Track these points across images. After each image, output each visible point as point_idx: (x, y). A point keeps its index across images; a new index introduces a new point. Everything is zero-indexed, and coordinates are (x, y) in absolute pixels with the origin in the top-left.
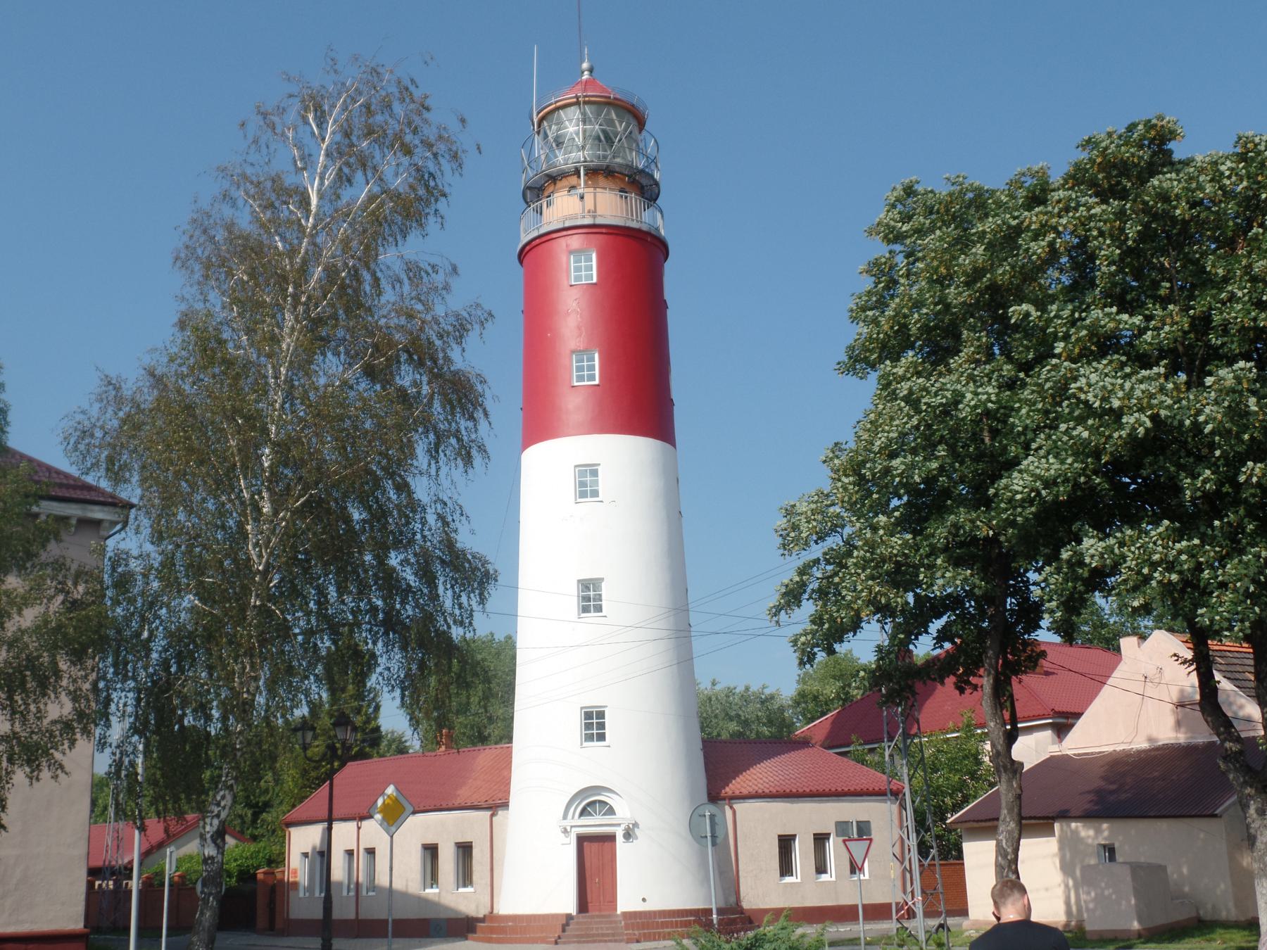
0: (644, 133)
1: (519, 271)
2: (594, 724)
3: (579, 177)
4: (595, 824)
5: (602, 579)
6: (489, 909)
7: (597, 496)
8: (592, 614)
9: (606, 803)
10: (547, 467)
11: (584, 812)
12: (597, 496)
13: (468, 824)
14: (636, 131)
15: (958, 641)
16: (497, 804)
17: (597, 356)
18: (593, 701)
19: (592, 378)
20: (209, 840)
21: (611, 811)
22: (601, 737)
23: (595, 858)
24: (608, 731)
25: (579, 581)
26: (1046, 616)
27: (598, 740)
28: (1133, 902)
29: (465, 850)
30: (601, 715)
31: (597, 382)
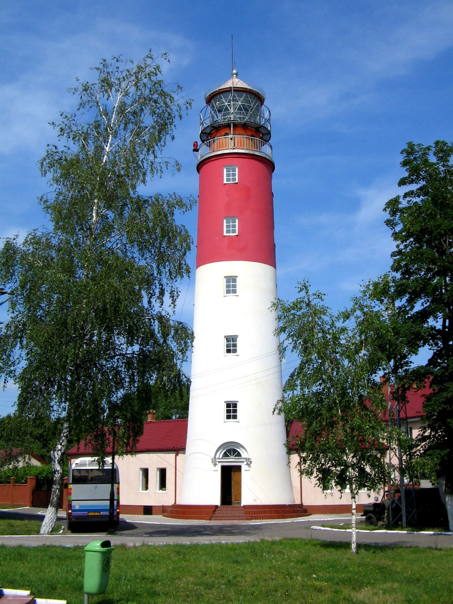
0: (263, 106)
1: (197, 176)
2: (232, 410)
3: (230, 129)
4: (231, 461)
5: (237, 277)
6: (174, 502)
7: (236, 293)
8: (231, 294)
9: (237, 451)
10: (210, 277)
11: (225, 455)
12: (236, 293)
13: (165, 460)
14: (260, 105)
15: (436, 323)
16: (178, 446)
17: (237, 169)
18: (231, 399)
19: (234, 179)
20: (57, 462)
21: (239, 455)
22: (235, 417)
23: (230, 477)
24: (238, 414)
25: (225, 336)
26: (209, 565)
27: (233, 418)
28: (223, 542)
29: (163, 472)
30: (235, 405)
31: (237, 234)
